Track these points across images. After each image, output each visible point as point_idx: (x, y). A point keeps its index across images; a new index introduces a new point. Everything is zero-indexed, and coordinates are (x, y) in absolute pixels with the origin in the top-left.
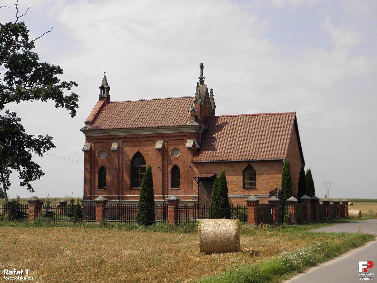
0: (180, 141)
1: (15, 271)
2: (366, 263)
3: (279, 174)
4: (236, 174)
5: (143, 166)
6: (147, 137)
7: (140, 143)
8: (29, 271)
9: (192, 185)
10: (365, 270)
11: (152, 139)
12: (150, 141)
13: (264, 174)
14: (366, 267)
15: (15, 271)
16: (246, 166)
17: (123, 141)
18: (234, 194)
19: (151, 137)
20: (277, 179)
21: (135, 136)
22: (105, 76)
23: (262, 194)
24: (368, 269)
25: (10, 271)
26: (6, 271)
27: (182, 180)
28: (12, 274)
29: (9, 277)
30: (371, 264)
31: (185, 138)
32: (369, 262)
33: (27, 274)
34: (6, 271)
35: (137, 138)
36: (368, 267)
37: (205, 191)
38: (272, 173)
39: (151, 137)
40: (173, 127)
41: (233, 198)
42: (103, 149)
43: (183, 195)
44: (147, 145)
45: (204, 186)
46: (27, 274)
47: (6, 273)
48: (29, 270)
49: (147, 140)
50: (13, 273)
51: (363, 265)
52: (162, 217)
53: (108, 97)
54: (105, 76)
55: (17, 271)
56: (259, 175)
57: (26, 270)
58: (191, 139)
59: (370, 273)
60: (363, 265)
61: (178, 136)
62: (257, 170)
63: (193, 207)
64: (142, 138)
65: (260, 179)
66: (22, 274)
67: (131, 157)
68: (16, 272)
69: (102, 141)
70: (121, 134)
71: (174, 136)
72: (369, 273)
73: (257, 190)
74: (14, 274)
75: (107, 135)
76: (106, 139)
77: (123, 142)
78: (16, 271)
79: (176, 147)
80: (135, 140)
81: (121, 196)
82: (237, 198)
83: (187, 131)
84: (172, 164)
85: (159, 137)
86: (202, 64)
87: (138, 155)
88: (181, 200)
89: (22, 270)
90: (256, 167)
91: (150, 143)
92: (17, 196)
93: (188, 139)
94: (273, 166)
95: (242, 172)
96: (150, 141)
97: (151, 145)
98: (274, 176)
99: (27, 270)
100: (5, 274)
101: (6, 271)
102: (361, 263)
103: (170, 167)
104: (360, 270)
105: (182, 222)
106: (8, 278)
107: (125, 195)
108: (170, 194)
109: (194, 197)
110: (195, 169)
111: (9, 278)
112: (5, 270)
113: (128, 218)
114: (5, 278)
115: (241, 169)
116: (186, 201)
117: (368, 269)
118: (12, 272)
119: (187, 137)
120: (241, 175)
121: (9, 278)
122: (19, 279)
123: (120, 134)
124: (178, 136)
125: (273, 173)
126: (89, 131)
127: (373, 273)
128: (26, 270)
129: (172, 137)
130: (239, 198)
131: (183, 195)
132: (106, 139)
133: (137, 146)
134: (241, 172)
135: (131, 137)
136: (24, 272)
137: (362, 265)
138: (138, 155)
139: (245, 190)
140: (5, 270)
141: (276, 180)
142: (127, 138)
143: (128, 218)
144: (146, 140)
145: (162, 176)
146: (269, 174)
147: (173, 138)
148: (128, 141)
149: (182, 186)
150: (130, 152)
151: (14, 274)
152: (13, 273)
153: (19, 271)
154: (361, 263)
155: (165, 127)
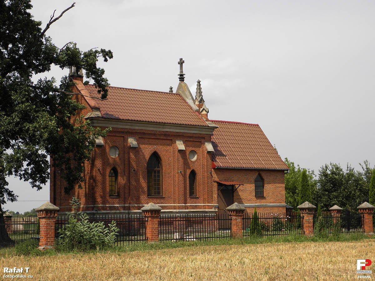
0: (197, 143)
1: (14, 269)
2: (364, 261)
4: (249, 182)
5: (156, 169)
6: (165, 135)
7: (157, 141)
8: (28, 269)
9: (212, 194)
10: (363, 268)
13: (270, 184)
14: (364, 265)
15: (14, 269)
18: (249, 203)
20: (280, 189)
21: (153, 133)
23: (270, 203)
24: (367, 267)
25: (10, 269)
26: (6, 269)
28: (12, 272)
29: (9, 275)
30: (369, 262)
31: (203, 140)
32: (367, 261)
33: (27, 272)
34: (6, 270)
35: (154, 135)
36: (366, 265)
37: (224, 200)
41: (249, 207)
43: (203, 204)
44: (164, 145)
46: (27, 272)
47: (6, 272)
48: (29, 268)
49: (165, 138)
50: (13, 271)
51: (361, 263)
55: (17, 269)
56: (267, 184)
57: (25, 268)
58: (208, 141)
59: (368, 271)
60: (361, 263)
63: (213, 219)
64: (161, 135)
65: (269, 188)
66: (22, 272)
67: (147, 156)
68: (16, 270)
69: (114, 135)
70: (137, 127)
72: (367, 271)
73: (266, 199)
74: (14, 272)
76: (119, 132)
78: (16, 269)
79: (193, 149)
80: (153, 137)
81: (126, 205)
82: (251, 207)
84: (190, 168)
85: (132, 133)
86: (181, 59)
87: (155, 157)
88: (162, 211)
89: (22, 268)
90: (264, 175)
91: (168, 142)
92: (49, 36)
93: (206, 141)
97: (168, 145)
98: (278, 185)
99: (27, 269)
100: (5, 272)
101: (6, 269)
102: (359, 261)
104: (359, 268)
105: (246, 236)
106: (8, 276)
107: (142, 204)
108: (189, 203)
109: (215, 207)
111: (9, 276)
112: (5, 268)
114: (5, 276)
117: (367, 267)
118: (12, 270)
119: (204, 139)
120: (253, 184)
121: (9, 276)
122: (19, 277)
123: (137, 128)
125: (277, 183)
126: (103, 119)
127: (371, 271)
128: (25, 268)
129: (190, 137)
130: (253, 207)
134: (253, 181)
136: (24, 271)
137: (360, 263)
138: (155, 157)
139: (257, 200)
140: (5, 268)
142: (144, 133)
145: (183, 182)
147: (191, 139)
150: (147, 150)
151: (14, 272)
152: (13, 271)
153: (19, 270)
154: (359, 261)
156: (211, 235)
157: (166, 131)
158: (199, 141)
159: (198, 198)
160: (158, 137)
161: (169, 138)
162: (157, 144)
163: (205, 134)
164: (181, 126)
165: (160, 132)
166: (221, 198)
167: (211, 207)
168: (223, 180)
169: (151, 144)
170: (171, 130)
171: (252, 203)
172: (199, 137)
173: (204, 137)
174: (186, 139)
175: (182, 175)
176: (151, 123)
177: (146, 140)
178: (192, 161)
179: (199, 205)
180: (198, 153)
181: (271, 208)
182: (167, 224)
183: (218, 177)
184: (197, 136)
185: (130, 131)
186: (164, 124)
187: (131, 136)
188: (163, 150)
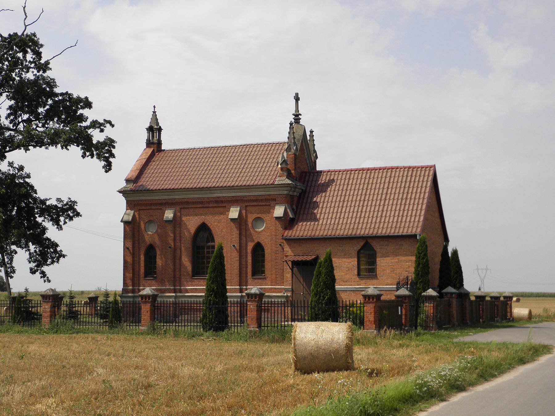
0: (265, 207)
3: (411, 256)
5: (210, 244)
6: (216, 202)
11: (224, 205)
16: (362, 243)
19: (222, 202)
20: (407, 263)
22: (154, 112)
23: (386, 285)
27: (268, 265)
31: (272, 203)
35: (202, 203)
38: (401, 255)
39: (222, 202)
41: (344, 291)
42: (152, 219)
44: (216, 214)
49: (216, 205)
52: (239, 319)
53: (159, 143)
54: (154, 112)
56: (382, 257)
61: (262, 200)
63: (284, 304)
64: (209, 202)
67: (193, 230)
71: (256, 200)
76: (156, 204)
77: (181, 208)
79: (259, 216)
80: (199, 206)
84: (253, 241)
85: (169, 204)
86: (297, 94)
87: (203, 228)
90: (376, 246)
94: (402, 245)
95: (356, 252)
98: (403, 258)
103: (250, 246)
105: (268, 327)
107: (185, 286)
108: (250, 286)
109: (286, 290)
113: (189, 321)
115: (355, 248)
119: (275, 201)
120: (354, 258)
123: (177, 197)
124: (262, 200)
125: (401, 255)
126: (131, 192)
132: (156, 204)
133: (202, 214)
134: (355, 253)
138: (203, 228)
142: (188, 203)
143: (189, 321)
144: (216, 205)
145: (238, 259)
147: (255, 203)
148: (188, 208)
149: (268, 273)
156: (90, 319)
157: (217, 197)
158: (267, 204)
159: (265, 278)
160: (207, 205)
161: (220, 205)
162: (205, 214)
163: (276, 195)
164: (241, 187)
165: (208, 199)
166: (298, 278)
167: (280, 290)
168: (300, 254)
169: (197, 214)
170: (224, 195)
171: (351, 285)
172: (267, 200)
173: (275, 199)
174: (246, 204)
175: (236, 249)
176: (184, 190)
177: (191, 210)
178: (256, 232)
179: (265, 288)
180: (266, 219)
181: (388, 292)
182: (266, 310)
183: (292, 251)
184: (263, 198)
185: (170, 201)
186: (209, 189)
187: (171, 208)
188: (213, 221)
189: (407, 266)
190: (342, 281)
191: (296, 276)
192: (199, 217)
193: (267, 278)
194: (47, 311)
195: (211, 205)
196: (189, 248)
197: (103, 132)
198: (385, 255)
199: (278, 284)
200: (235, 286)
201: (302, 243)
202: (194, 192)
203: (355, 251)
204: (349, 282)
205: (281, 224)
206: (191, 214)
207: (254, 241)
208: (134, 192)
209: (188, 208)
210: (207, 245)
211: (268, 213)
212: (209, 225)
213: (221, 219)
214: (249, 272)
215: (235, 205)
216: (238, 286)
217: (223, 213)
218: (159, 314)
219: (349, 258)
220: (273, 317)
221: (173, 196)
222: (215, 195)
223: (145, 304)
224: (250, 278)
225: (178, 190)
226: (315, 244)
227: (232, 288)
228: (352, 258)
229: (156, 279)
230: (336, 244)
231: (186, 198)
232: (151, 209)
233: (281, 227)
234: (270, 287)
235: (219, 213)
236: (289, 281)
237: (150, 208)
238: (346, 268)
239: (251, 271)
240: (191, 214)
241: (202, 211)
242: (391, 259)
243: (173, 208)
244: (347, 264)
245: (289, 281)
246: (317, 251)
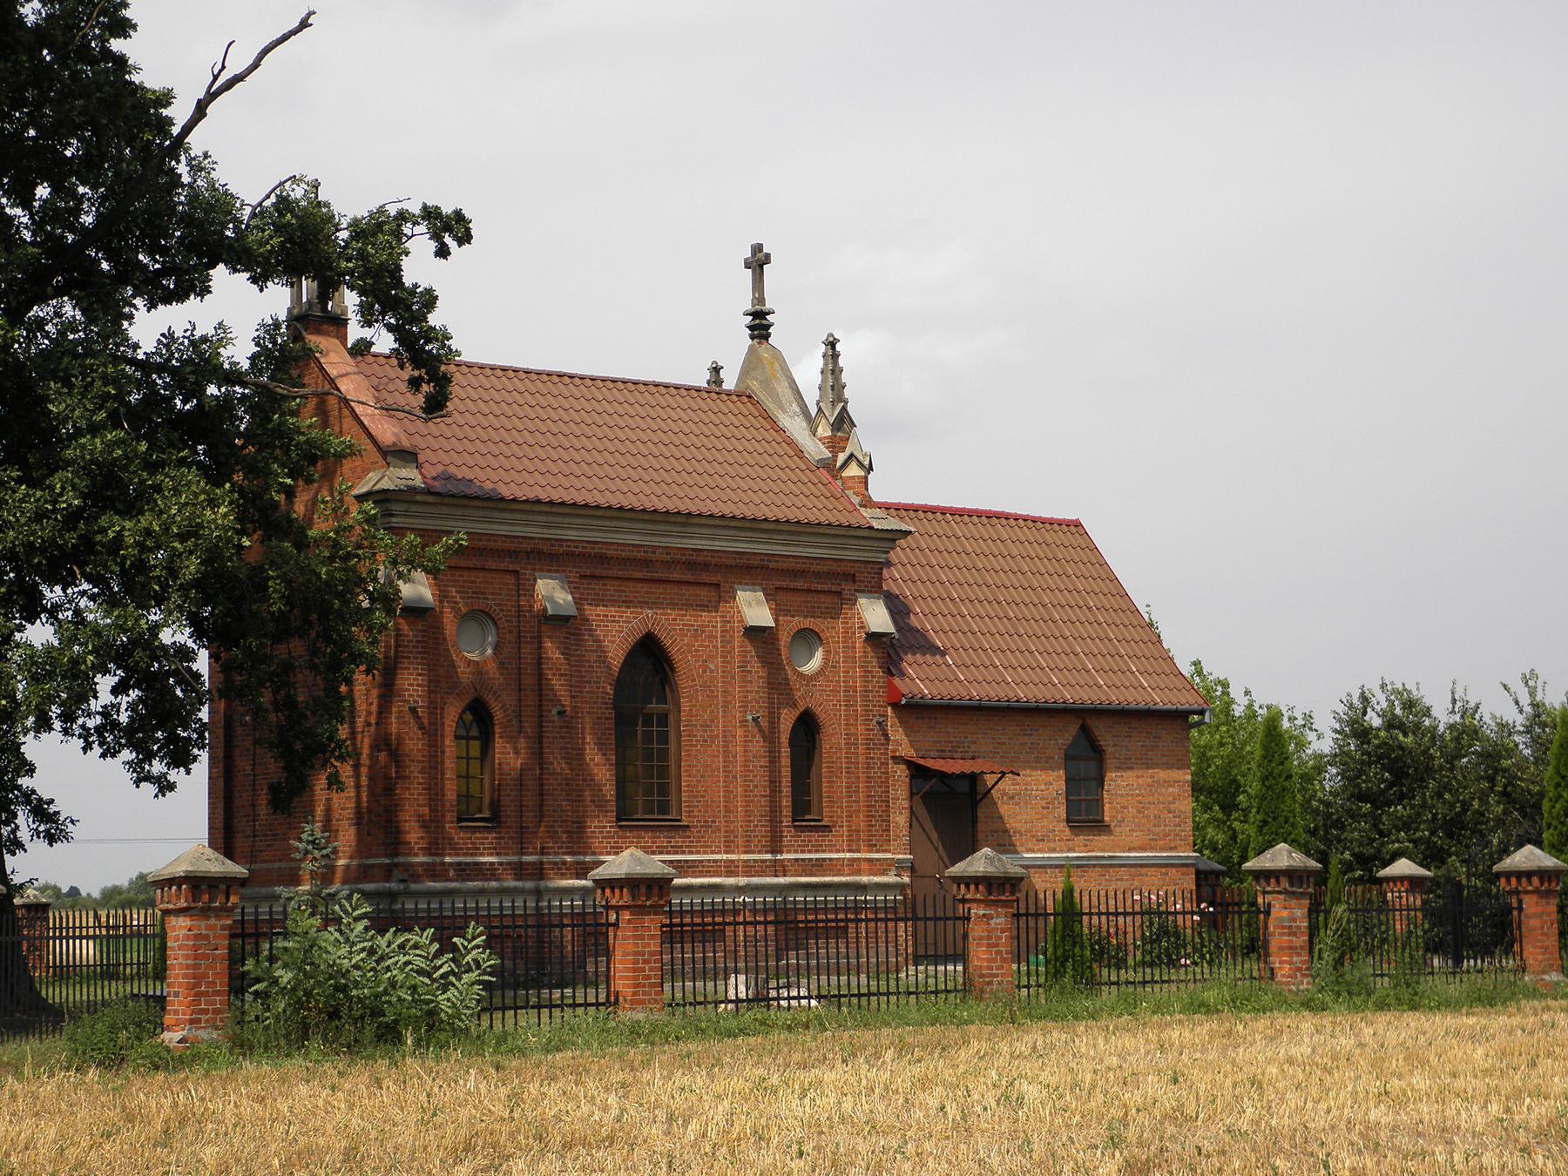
0: (823, 598)
3: (1178, 769)
5: (654, 706)
6: (691, 565)
7: (658, 590)
12: (705, 584)
17: (582, 571)
18: (1039, 851)
20: (1171, 790)
23: (1130, 850)
31: (847, 587)
35: (646, 563)
37: (935, 836)
38: (1156, 764)
39: (706, 566)
40: (726, 523)
45: (929, 813)
49: (689, 577)
52: (772, 963)
56: (1118, 768)
58: (870, 592)
62: (1110, 750)
63: (891, 914)
67: (616, 654)
75: (504, 530)
79: (808, 623)
80: (639, 575)
82: (1051, 866)
83: (853, 555)
85: (552, 558)
86: (757, 248)
88: (676, 881)
90: (1105, 735)
93: (863, 591)
94: (1160, 738)
96: (705, 584)
97: (704, 607)
98: (1163, 775)
103: (787, 719)
105: (1028, 987)
107: (594, 854)
109: (899, 867)
110: (897, 734)
113: (843, 969)
116: (702, 887)
119: (854, 582)
120: (1059, 770)
123: (571, 535)
126: (430, 499)
131: (848, 855)
133: (643, 604)
134: (1058, 757)
135: (580, 553)
139: (1076, 835)
141: (1170, 794)
142: (602, 559)
143: (843, 969)
146: (1147, 768)
148: (602, 578)
155: (703, 521)
157: (693, 550)
158: (834, 588)
159: (827, 828)
165: (667, 554)
166: (924, 830)
170: (717, 545)
171: (1054, 850)
175: (761, 731)
178: (801, 675)
183: (911, 741)
186: (686, 520)
187: (550, 571)
189: (1171, 799)
190: (1033, 836)
191: (918, 821)
192: (637, 613)
193: (835, 826)
194: (1300, 927)
195: (676, 576)
196: (607, 719)
197: (445, 258)
198: (1125, 766)
199: (876, 845)
200: (760, 852)
201: (936, 718)
202: (657, 527)
203: (1060, 749)
204: (1048, 841)
205: (878, 658)
206: (612, 601)
207: (796, 706)
208: (438, 500)
209: (602, 578)
210: (645, 711)
211: (832, 618)
212: (668, 642)
213: (702, 626)
214: (787, 806)
215: (746, 584)
216: (767, 852)
217: (707, 606)
218: (1043, 935)
219: (1047, 768)
220: (853, 952)
221: (558, 532)
222: (689, 541)
223: (1544, 900)
224: (787, 827)
225: (601, 513)
226: (966, 724)
227: (755, 861)
228: (1053, 771)
229: (500, 827)
230: (1017, 726)
231: (597, 543)
232: (483, 569)
233: (880, 667)
234: (848, 855)
235: (697, 605)
236: (903, 836)
237: (479, 564)
238: (1041, 799)
239: (790, 804)
240: (612, 601)
241: (645, 592)
242: (1138, 777)
243: (557, 571)
244: (1043, 787)
245: (903, 836)
246: (973, 747)
